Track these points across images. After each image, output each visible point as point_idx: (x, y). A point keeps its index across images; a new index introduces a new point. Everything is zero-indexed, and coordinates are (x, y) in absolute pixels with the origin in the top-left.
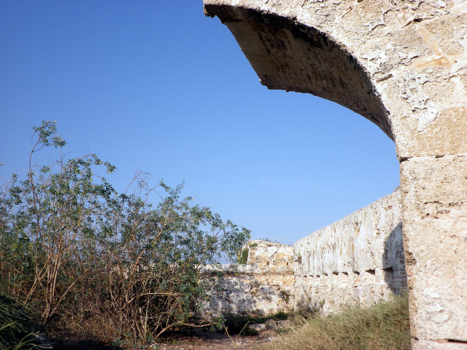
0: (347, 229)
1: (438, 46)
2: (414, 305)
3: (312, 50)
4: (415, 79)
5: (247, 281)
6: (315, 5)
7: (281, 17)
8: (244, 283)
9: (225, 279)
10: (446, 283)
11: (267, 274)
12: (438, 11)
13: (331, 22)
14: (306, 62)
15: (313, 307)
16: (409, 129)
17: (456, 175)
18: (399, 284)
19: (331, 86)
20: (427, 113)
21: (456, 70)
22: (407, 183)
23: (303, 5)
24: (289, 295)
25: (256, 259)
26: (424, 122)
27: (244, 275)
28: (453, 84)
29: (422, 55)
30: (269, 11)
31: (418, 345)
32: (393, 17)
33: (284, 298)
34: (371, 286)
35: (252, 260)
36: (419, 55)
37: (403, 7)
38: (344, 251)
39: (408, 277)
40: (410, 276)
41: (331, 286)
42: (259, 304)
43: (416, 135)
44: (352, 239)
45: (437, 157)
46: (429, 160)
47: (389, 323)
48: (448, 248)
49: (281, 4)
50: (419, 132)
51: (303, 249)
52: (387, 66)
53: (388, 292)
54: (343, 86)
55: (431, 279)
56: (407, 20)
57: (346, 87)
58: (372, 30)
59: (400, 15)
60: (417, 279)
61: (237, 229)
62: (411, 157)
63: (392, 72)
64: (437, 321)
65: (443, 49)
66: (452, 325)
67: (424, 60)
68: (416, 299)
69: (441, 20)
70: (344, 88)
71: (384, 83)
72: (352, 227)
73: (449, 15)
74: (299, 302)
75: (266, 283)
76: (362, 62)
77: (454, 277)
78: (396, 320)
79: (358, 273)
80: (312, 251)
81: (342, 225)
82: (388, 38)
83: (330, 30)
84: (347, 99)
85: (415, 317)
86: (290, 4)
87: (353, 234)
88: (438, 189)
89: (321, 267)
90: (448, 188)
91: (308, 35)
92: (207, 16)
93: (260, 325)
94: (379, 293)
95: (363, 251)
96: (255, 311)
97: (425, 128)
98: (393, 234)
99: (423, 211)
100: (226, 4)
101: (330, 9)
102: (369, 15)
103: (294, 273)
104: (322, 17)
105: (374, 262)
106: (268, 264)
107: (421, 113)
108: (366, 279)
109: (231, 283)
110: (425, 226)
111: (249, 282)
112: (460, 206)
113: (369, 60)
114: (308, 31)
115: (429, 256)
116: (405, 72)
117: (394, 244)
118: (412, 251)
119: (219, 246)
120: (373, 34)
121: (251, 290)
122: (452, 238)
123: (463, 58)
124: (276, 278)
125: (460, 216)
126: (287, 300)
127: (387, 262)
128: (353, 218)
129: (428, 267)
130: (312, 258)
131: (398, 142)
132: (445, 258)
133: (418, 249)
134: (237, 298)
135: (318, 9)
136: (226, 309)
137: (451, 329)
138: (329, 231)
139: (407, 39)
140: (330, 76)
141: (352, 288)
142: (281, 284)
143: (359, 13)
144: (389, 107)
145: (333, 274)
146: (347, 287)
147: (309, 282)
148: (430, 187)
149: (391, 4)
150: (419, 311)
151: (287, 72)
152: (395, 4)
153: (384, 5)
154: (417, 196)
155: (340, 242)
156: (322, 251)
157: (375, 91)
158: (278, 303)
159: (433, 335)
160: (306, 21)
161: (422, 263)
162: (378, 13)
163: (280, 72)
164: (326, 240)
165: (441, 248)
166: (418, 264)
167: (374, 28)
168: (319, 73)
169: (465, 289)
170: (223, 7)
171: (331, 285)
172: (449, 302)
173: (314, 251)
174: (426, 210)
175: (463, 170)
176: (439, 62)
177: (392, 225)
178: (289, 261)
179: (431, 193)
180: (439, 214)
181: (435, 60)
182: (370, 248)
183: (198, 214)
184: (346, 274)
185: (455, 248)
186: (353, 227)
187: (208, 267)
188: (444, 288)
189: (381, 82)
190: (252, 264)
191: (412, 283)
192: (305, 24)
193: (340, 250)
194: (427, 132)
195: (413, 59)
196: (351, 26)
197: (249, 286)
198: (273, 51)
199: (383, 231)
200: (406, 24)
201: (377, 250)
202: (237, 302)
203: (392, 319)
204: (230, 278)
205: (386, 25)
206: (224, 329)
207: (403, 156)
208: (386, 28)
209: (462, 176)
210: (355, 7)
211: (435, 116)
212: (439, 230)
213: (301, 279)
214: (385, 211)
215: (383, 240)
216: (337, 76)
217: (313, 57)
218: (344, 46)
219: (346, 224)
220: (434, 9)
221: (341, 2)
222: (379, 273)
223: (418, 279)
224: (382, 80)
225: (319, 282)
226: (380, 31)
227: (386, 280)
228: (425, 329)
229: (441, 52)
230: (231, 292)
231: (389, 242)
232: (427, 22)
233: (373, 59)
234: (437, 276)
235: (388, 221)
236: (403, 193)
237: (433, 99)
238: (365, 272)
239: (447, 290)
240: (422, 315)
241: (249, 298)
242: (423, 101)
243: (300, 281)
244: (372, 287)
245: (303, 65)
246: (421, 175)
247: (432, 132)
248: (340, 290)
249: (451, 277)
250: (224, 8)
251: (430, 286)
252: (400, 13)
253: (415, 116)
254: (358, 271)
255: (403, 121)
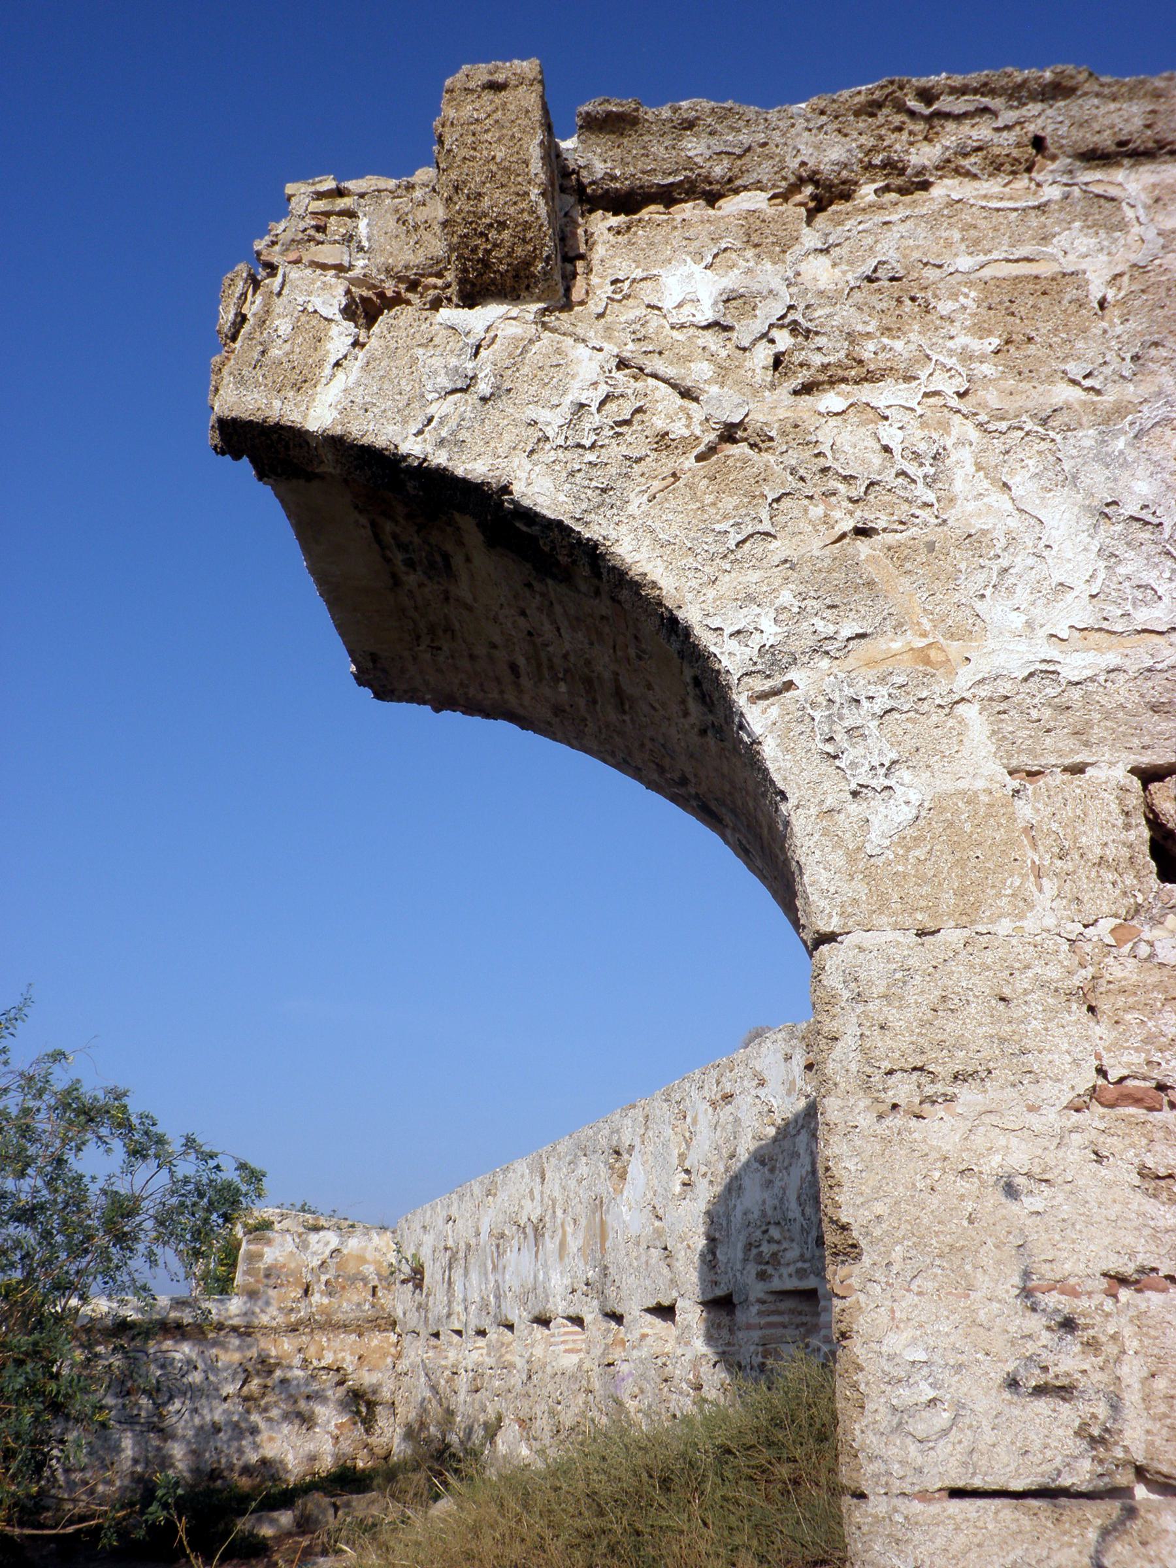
0: (583, 1170)
1: (920, 611)
2: (855, 1386)
3: (537, 586)
4: (858, 701)
5: (230, 1356)
6: (569, 455)
7: (464, 481)
8: (219, 1364)
9: (151, 1351)
10: (946, 1313)
11: (301, 1328)
12: (918, 512)
13: (615, 511)
14: (514, 622)
15: (462, 1442)
16: (841, 847)
17: (972, 990)
18: (752, 1348)
19: (582, 703)
20: (892, 801)
21: (970, 684)
22: (837, 1010)
23: (532, 452)
24: (376, 1404)
25: (267, 1276)
26: (885, 827)
27: (222, 1333)
28: (961, 722)
29: (877, 633)
30: (425, 460)
31: (866, 1515)
32: (796, 513)
33: (358, 1413)
34: (659, 1362)
35: (252, 1280)
36: (869, 631)
37: (824, 489)
38: (573, 1245)
39: (835, 1301)
40: (844, 1298)
41: (526, 1367)
42: (271, 1439)
43: (861, 865)
44: (598, 1204)
45: (921, 933)
46: (899, 943)
47: (731, 1477)
48: (952, 1209)
49: (463, 441)
50: (871, 856)
51: (428, 1240)
52: (780, 657)
53: (715, 1379)
54: (622, 704)
55: (904, 1304)
56: (836, 529)
57: (631, 707)
58: (737, 545)
59: (817, 511)
60: (863, 1305)
61: (218, 1167)
62: (848, 933)
63: (792, 675)
64: (920, 1436)
65: (932, 621)
66: (960, 1442)
67: (884, 647)
68: (862, 1370)
69: (926, 539)
70: (624, 712)
71: (769, 707)
72: (602, 1165)
73: (945, 528)
74: (409, 1426)
75: (297, 1361)
76: (706, 639)
77: (968, 1296)
78: (752, 1463)
79: (618, 1318)
80: (462, 1246)
81: (568, 1159)
82: (782, 574)
83: (613, 535)
84: (627, 747)
85: (857, 1426)
86: (492, 444)
87: (605, 1187)
88: (924, 1031)
89: (492, 1298)
90: (952, 1026)
91: (541, 542)
92: (217, 453)
93: (275, 1514)
94: (688, 1382)
95: (638, 1244)
96: (254, 1466)
97: (887, 848)
98: (735, 1184)
99: (882, 1095)
100: (289, 424)
101: (614, 471)
102: (729, 502)
103: (394, 1324)
104: (589, 492)
105: (671, 1280)
106: (306, 1292)
107: (877, 802)
108: (644, 1336)
109: (172, 1364)
110: (886, 1141)
111: (236, 1357)
112: (982, 1080)
113: (727, 632)
114: (543, 532)
115: (899, 1234)
116: (832, 677)
117: (737, 1218)
118: (851, 1221)
119: (149, 1224)
120: (739, 557)
121: (245, 1388)
122: (962, 1178)
123: (985, 651)
124: (332, 1344)
125: (983, 1109)
126: (368, 1423)
127: (714, 1278)
128: (606, 1132)
129: (895, 1269)
130: (461, 1271)
131: (811, 885)
132: (942, 1238)
133: (866, 1213)
134: (192, 1419)
135: (577, 467)
136: (147, 1463)
137: (958, 1456)
138: (522, 1176)
139: (835, 583)
140: (586, 670)
141: (595, 1368)
142: (349, 1362)
143: (699, 493)
144: (785, 779)
145: (533, 1322)
146: (580, 1367)
147: (450, 1354)
148: (901, 1023)
149: (790, 478)
150: (870, 1406)
151: (445, 648)
152: (802, 479)
153: (771, 478)
154: (864, 1051)
155: (559, 1213)
156: (498, 1246)
157: (741, 727)
158: (337, 1432)
159: (908, 1480)
160: (540, 500)
161: (879, 1255)
162: (754, 497)
163: (421, 648)
164: (512, 1209)
165: (933, 1207)
166: (866, 1259)
167: (744, 541)
168: (550, 660)
169: (996, 1329)
170: (276, 432)
171: (524, 1361)
172: (953, 1373)
173: (468, 1246)
174: (890, 1093)
175: (991, 973)
176: (922, 656)
177: (732, 1156)
178: (380, 1280)
179: (904, 1042)
180: (926, 1106)
181: (912, 649)
182: (659, 1233)
183: (85, 1113)
184: (578, 1321)
185: (969, 1206)
186: (606, 1163)
187: (101, 1306)
188: (939, 1331)
189: (763, 703)
190: (252, 1295)
191: (848, 1319)
192: (538, 509)
193: (557, 1240)
194: (891, 857)
195: (851, 642)
196: (675, 530)
197: (235, 1373)
198: (411, 579)
199: (704, 1175)
200: (833, 539)
201: (682, 1239)
202: (191, 1433)
203: (741, 1462)
204: (168, 1344)
205: (778, 535)
206: (170, 1523)
207: (825, 928)
208: (775, 544)
209: (988, 991)
210: (689, 474)
211: (914, 812)
212: (927, 1155)
213: (421, 1342)
214: (710, 1110)
215: (703, 1207)
216: (607, 675)
217: (540, 609)
218: (654, 585)
219: (580, 1153)
220: (905, 506)
221: (647, 456)
222: (689, 1317)
223: (867, 1305)
224: (764, 696)
225: (484, 1351)
226: (758, 551)
227: (710, 1339)
228: (885, 1462)
229: (928, 629)
230: (171, 1398)
231: (722, 1210)
232: (889, 538)
233: (739, 632)
234: (920, 1294)
235: (721, 1142)
236: (824, 1040)
237: (910, 764)
238: (643, 1313)
239: (947, 1335)
240: (878, 1418)
241: (235, 1418)
242: (882, 765)
243: (416, 1352)
244: (665, 1364)
245: (502, 633)
246: (877, 986)
247: (907, 860)
248: (557, 1379)
249: (959, 1296)
250: (281, 435)
251: (902, 1325)
252: (817, 506)
253: (860, 808)
254: (619, 1310)
255: (825, 823)
